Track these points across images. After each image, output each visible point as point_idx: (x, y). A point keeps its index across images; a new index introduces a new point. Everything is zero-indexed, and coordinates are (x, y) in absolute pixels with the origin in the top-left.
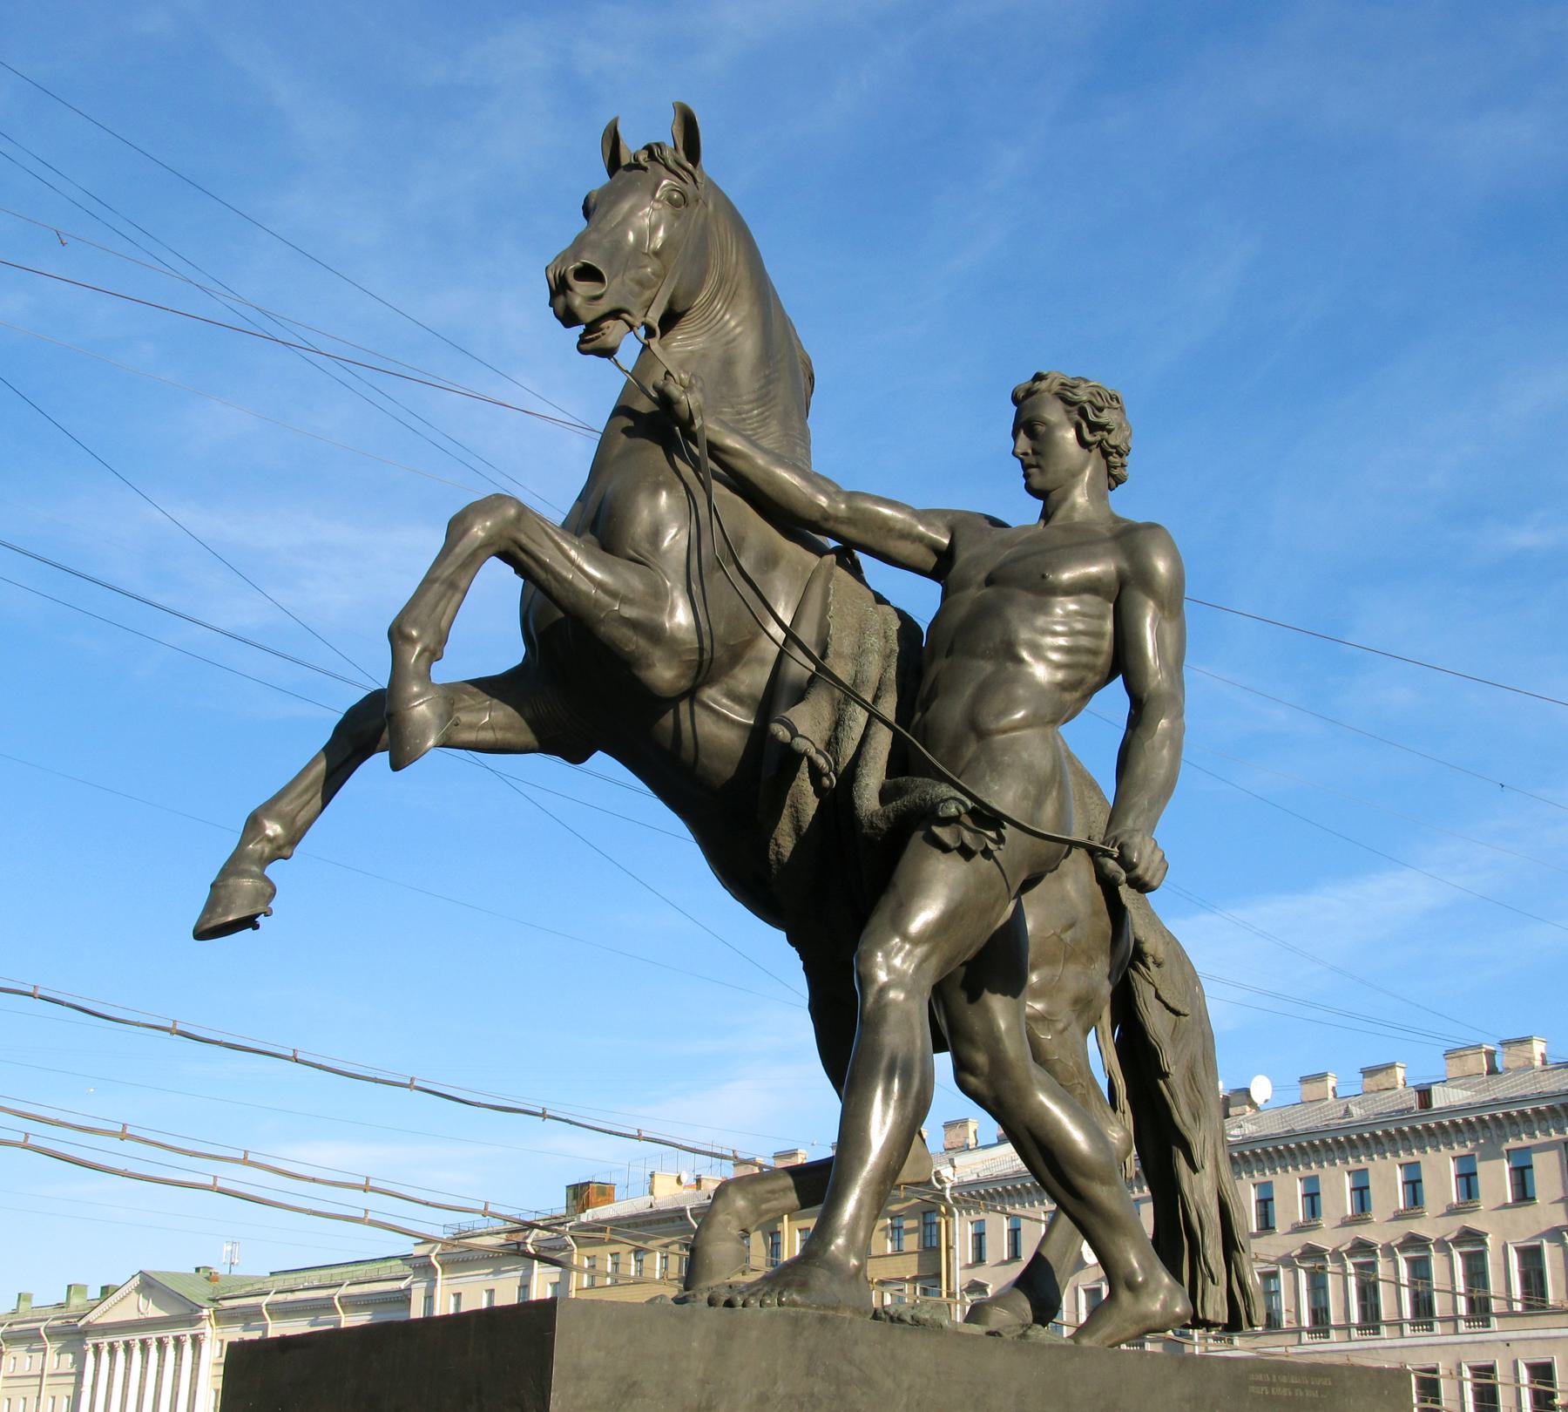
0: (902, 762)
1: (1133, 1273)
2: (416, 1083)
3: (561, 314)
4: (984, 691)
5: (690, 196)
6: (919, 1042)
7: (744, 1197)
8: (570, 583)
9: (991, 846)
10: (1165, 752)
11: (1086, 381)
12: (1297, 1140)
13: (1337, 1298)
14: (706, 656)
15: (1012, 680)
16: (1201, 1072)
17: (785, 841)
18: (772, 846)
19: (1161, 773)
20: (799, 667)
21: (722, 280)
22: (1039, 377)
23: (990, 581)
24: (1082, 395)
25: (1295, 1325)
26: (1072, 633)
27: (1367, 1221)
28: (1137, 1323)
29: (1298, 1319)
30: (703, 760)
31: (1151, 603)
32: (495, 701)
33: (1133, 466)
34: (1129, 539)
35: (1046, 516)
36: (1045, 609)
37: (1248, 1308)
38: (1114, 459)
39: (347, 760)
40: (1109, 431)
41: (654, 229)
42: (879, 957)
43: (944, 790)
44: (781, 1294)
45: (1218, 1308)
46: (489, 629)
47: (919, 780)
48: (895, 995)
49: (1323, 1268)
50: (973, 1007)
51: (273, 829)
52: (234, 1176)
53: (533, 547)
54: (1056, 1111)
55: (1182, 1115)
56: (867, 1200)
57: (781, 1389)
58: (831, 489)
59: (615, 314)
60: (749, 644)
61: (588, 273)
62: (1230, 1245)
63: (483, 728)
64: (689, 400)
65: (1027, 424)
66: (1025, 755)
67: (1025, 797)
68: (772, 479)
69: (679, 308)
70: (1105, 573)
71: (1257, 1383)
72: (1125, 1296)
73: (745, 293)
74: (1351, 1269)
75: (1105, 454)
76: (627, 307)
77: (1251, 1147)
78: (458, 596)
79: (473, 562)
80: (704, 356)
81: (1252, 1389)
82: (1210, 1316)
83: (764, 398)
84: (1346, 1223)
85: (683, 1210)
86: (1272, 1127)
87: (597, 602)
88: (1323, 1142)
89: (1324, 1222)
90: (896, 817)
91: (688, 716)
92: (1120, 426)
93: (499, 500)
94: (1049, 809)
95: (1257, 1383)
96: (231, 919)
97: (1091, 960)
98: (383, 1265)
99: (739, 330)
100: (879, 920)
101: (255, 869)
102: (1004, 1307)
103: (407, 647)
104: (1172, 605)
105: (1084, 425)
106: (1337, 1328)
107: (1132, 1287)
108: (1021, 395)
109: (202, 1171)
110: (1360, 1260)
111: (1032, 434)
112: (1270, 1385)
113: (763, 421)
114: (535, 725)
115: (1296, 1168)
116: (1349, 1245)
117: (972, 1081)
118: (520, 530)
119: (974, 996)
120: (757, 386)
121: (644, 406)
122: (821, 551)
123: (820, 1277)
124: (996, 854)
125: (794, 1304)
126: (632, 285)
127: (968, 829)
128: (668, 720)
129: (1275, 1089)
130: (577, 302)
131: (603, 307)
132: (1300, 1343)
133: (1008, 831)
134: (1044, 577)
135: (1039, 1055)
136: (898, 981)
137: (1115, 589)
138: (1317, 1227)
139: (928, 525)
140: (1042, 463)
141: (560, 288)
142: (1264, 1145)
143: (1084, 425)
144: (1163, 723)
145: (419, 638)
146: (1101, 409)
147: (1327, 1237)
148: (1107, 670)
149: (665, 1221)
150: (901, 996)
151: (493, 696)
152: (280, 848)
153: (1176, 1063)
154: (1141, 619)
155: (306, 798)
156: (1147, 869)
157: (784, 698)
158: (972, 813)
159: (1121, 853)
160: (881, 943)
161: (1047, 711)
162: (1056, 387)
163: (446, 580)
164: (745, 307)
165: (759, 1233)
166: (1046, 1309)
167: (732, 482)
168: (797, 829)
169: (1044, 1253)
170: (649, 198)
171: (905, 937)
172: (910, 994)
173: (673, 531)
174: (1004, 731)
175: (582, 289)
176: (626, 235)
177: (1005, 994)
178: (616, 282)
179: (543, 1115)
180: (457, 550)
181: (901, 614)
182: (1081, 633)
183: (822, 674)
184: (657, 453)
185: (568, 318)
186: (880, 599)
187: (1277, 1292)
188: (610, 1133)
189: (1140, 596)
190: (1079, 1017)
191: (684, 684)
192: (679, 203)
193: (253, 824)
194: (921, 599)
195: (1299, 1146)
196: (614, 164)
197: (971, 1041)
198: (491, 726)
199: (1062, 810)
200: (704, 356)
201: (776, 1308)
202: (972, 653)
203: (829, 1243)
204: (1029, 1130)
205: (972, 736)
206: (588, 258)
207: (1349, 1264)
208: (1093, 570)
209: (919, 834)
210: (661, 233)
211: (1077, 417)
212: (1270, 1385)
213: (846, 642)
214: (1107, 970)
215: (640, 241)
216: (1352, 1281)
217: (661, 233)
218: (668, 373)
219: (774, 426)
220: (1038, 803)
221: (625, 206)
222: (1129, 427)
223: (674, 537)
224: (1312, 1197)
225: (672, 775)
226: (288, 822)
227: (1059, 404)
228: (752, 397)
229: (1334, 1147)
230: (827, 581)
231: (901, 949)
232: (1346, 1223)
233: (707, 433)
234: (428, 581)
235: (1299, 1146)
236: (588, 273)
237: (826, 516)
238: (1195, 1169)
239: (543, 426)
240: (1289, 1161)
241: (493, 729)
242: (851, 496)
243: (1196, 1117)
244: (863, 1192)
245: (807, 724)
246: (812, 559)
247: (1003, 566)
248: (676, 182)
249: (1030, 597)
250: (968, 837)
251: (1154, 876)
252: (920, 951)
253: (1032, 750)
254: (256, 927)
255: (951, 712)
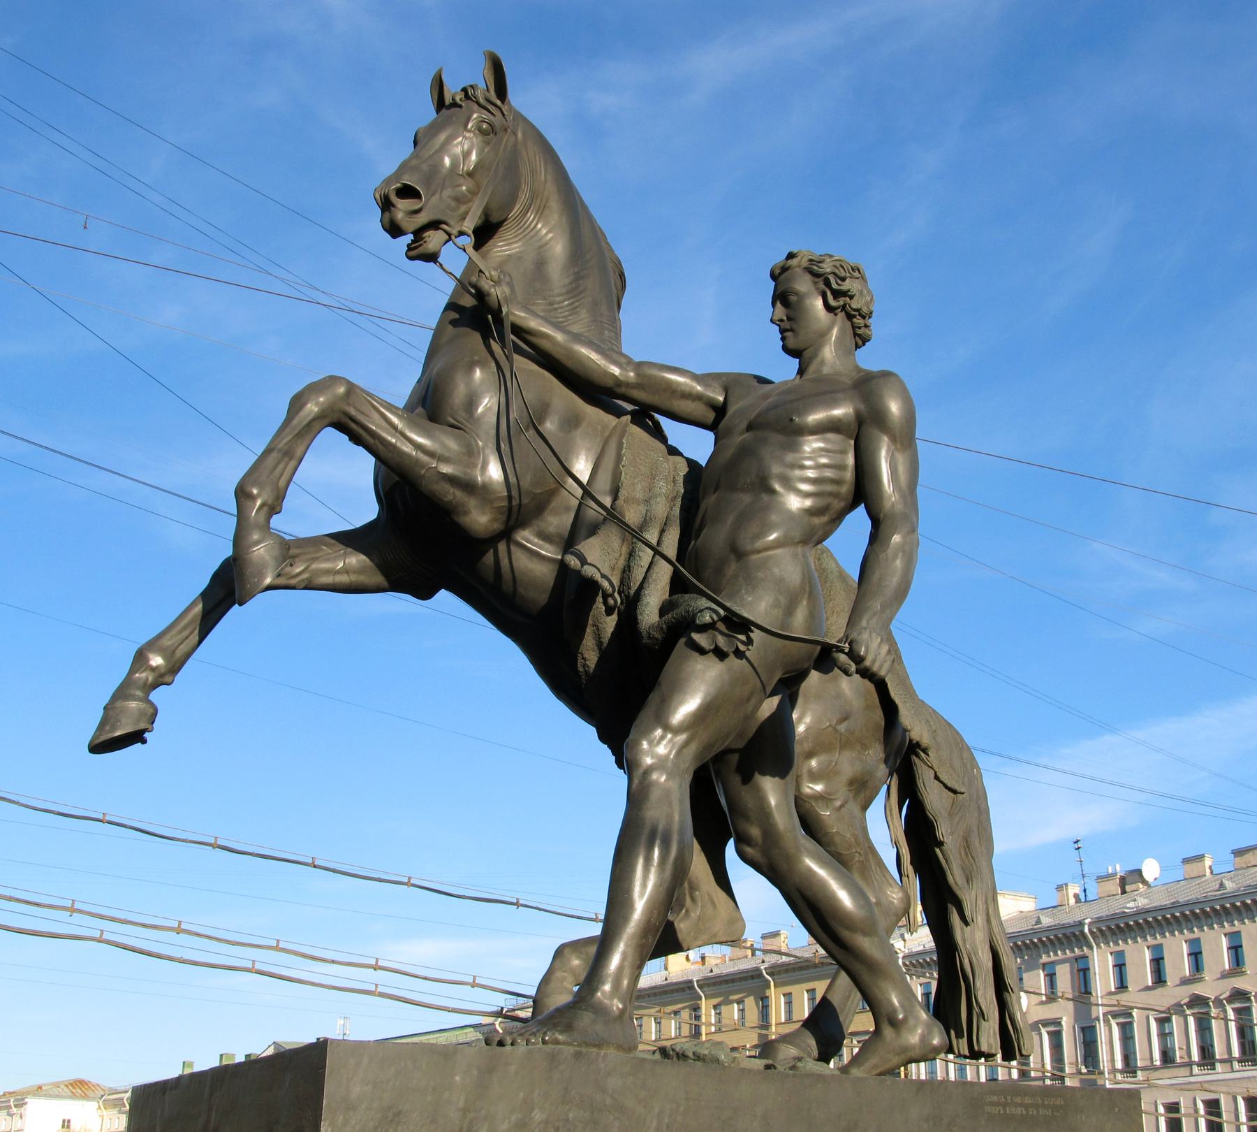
0: (678, 585)
1: (895, 1011)
2: (412, 881)
3: (388, 227)
4: (744, 517)
5: (497, 125)
6: (676, 818)
7: (578, 958)
8: (394, 446)
9: (742, 648)
10: (898, 563)
11: (831, 256)
12: (1181, 909)
13: (1220, 1036)
14: (514, 503)
15: (767, 508)
16: (975, 841)
17: (590, 655)
18: (580, 660)
19: (894, 581)
20: (593, 512)
21: (533, 196)
22: (791, 256)
23: (750, 428)
24: (827, 268)
25: (1186, 1060)
26: (818, 467)
27: (1243, 973)
28: (899, 1054)
29: (1189, 1055)
30: (521, 590)
31: (886, 439)
32: (349, 550)
33: (877, 327)
34: (867, 387)
35: (801, 372)
36: (794, 447)
37: (1018, 1039)
38: (858, 321)
39: (218, 605)
40: (851, 297)
41: (466, 155)
42: (645, 745)
43: (704, 603)
44: (545, 1033)
45: (992, 1041)
46: (337, 489)
47: (687, 596)
48: (660, 778)
49: (1208, 1014)
50: (745, 788)
51: (157, 661)
52: (267, 960)
53: (360, 418)
54: (821, 872)
55: (955, 877)
56: (630, 952)
57: (538, 1116)
58: (623, 360)
59: (434, 225)
60: (551, 494)
61: (407, 192)
62: (1001, 987)
63: (338, 572)
64: (497, 292)
65: (782, 297)
66: (776, 571)
67: (776, 605)
68: (571, 354)
69: (495, 219)
70: (845, 415)
71: (993, 1104)
72: (888, 1032)
73: (555, 204)
74: (1231, 1015)
75: (850, 317)
76: (444, 218)
77: (1144, 916)
78: (293, 463)
79: (309, 431)
80: (520, 258)
81: (988, 1109)
82: (984, 1048)
83: (575, 290)
84: (1225, 975)
85: (691, 982)
86: (1162, 900)
87: (417, 461)
88: (1203, 910)
89: (1207, 975)
90: (669, 628)
91: (506, 555)
92: (861, 292)
93: (333, 380)
94: (800, 616)
95: (993, 1104)
96: (118, 733)
97: (865, 747)
98: (461, 1032)
99: (550, 235)
100: (646, 715)
101: (139, 693)
102: (791, 1043)
103: (249, 503)
104: (905, 438)
105: (829, 293)
106: (1222, 1061)
107: (894, 1024)
108: (777, 272)
109: (242, 956)
110: (1237, 1005)
111: (786, 304)
112: (1005, 1105)
113: (574, 310)
114: (384, 568)
115: (1181, 932)
116: (1228, 994)
117: (749, 850)
118: (349, 404)
119: (747, 779)
120: (567, 281)
121: (468, 301)
122: (618, 413)
123: (585, 1019)
124: (748, 653)
125: (557, 1042)
126: (449, 201)
127: (722, 633)
128: (489, 558)
129: (1163, 869)
130: (400, 216)
131: (422, 219)
132: (1191, 1075)
133: (756, 635)
134: (791, 420)
135: (810, 825)
136: (661, 764)
137: (854, 426)
138: (1201, 979)
139: (706, 385)
140: (794, 327)
141: (386, 205)
142: (1154, 914)
143: (829, 293)
144: (896, 538)
145: (259, 495)
146: (843, 279)
147: (1210, 987)
148: (851, 497)
149: (677, 991)
150: (663, 779)
151: (347, 546)
152: (162, 676)
153: (952, 834)
154: (880, 449)
155: (185, 633)
156: (874, 661)
157: (583, 532)
158: (724, 620)
159: (851, 649)
160: (647, 732)
161: (797, 534)
162: (805, 263)
163: (286, 449)
164: (555, 215)
165: (752, 998)
166: (829, 1045)
167: (541, 359)
168: (599, 644)
169: (829, 997)
170: (461, 129)
171: (667, 728)
172: (670, 775)
173: (486, 400)
174: (759, 552)
175: (403, 205)
176: (443, 160)
177: (773, 775)
178: (434, 200)
179: (517, 904)
180: (295, 422)
181: (688, 460)
182: (825, 466)
183: (613, 516)
184: (476, 337)
185: (394, 230)
186: (673, 451)
187: (1171, 1033)
188: (572, 917)
189: (875, 432)
190: (855, 797)
191: (497, 527)
192: (488, 133)
193: (140, 658)
194: (697, 444)
195: (1183, 914)
196: (440, 104)
197: (747, 818)
198: (345, 571)
199: (813, 616)
200: (518, 258)
201: (541, 1045)
202: (733, 488)
203: (596, 990)
204: (800, 892)
205: (732, 557)
206: (407, 180)
207: (1229, 1009)
208: (838, 412)
209: (682, 641)
210: (474, 157)
211: (823, 287)
212: (1005, 1105)
213: (639, 487)
214: (882, 755)
215: (455, 165)
216: (1232, 1025)
217: (474, 157)
218: (481, 271)
219: (584, 314)
220: (790, 610)
221: (442, 137)
222: (869, 292)
223: (487, 404)
224: (1196, 956)
225: (500, 604)
226: (168, 654)
227: (808, 277)
228: (563, 291)
229: (1212, 914)
230: (622, 436)
231: (662, 738)
232: (1225, 975)
233: (511, 318)
234: (267, 452)
235: (1183, 914)
236: (407, 192)
237: (618, 382)
238: (967, 924)
239: (382, 320)
240: (1175, 926)
241: (347, 572)
242: (639, 365)
243: (969, 880)
244: (626, 945)
245: (600, 557)
246: (611, 420)
247: (759, 415)
248: (485, 115)
249: (780, 438)
250: (721, 641)
251: (880, 667)
252: (682, 738)
253: (786, 567)
254: (144, 741)
255: (715, 537)
